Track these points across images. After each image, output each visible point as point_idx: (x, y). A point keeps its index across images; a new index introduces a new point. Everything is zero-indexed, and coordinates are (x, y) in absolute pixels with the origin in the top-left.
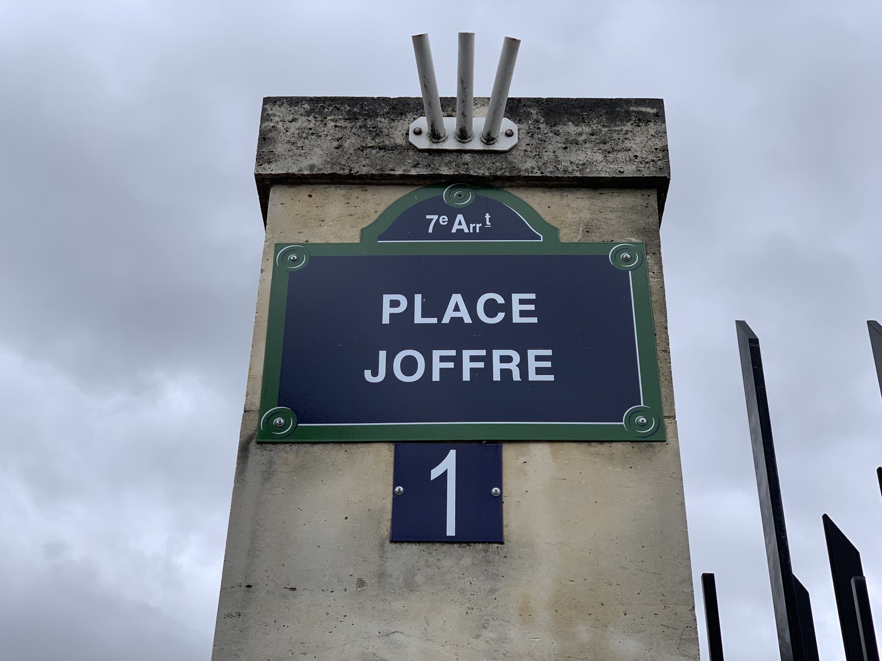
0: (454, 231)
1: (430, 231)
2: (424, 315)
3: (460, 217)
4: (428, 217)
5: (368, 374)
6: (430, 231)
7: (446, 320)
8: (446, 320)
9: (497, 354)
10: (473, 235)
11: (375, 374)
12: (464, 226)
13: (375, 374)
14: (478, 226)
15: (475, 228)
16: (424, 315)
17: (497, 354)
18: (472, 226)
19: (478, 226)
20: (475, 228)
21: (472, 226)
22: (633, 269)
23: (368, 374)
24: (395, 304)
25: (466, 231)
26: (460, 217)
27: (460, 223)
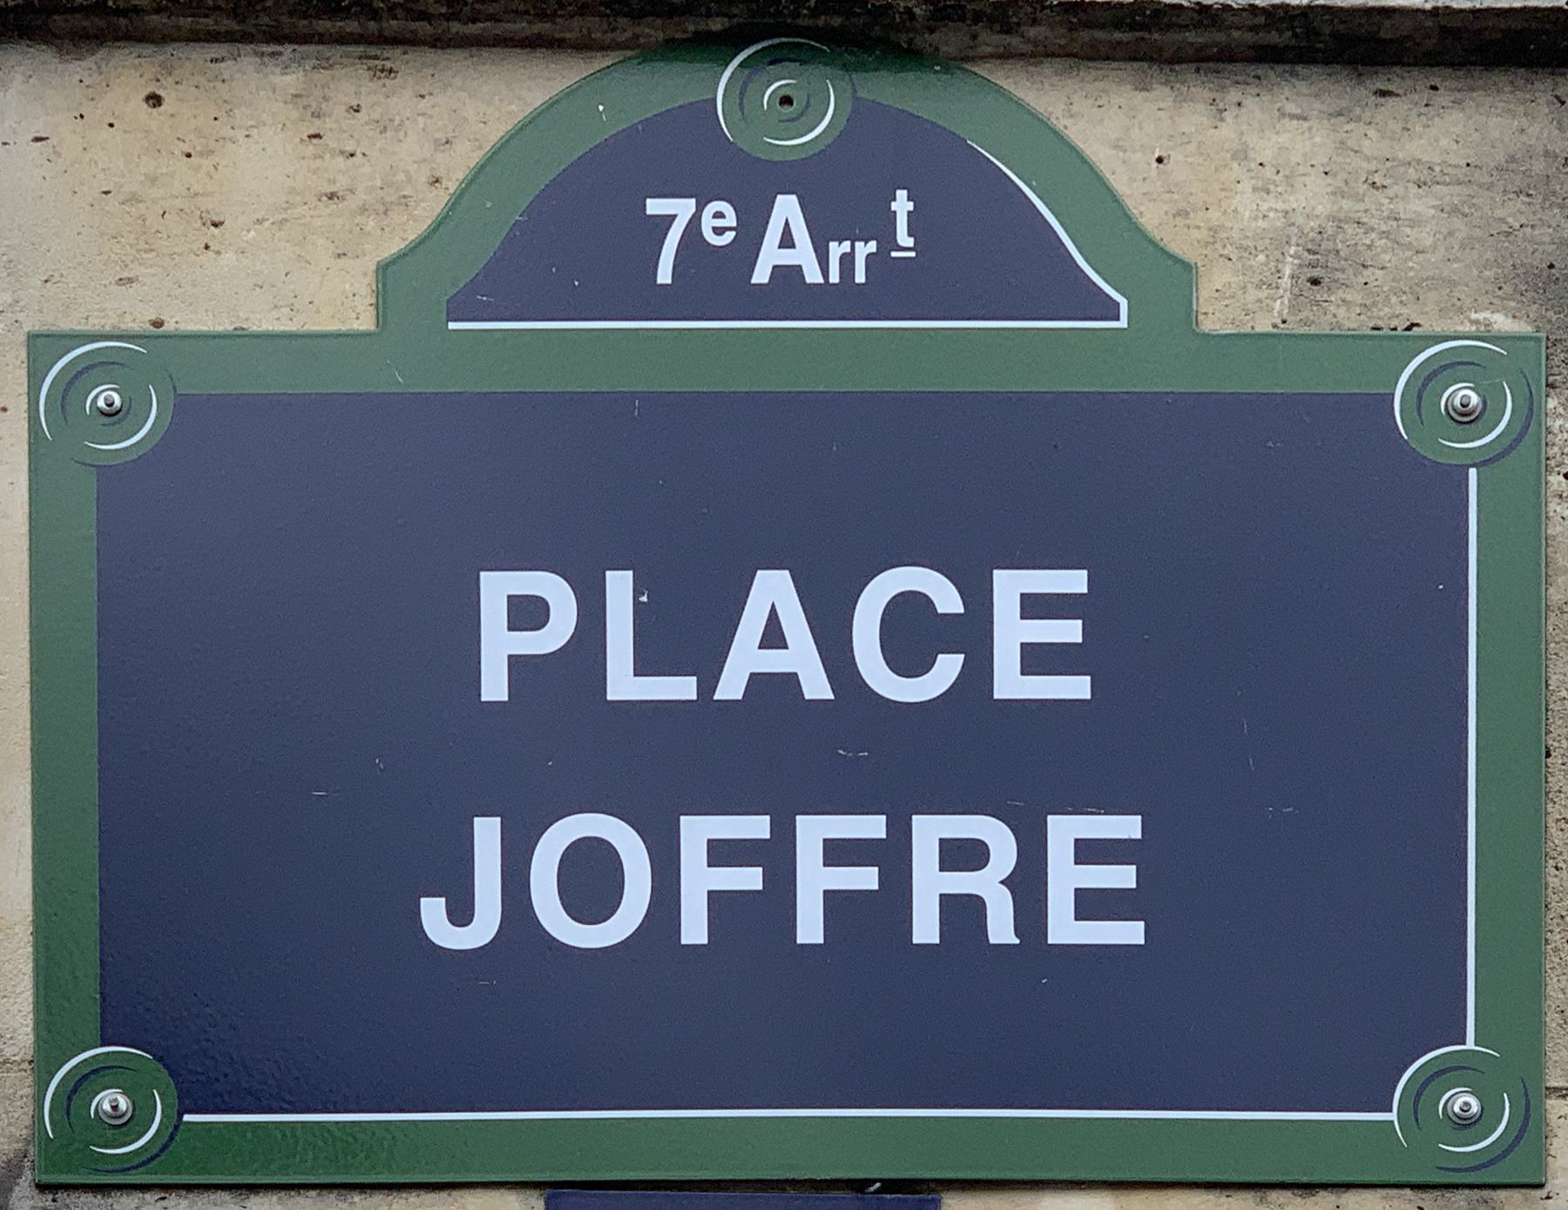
2: (645, 666)
5: (433, 911)
9: (929, 831)
11: (461, 914)
12: (803, 255)
13: (461, 914)
14: (864, 250)
15: (847, 261)
16: (645, 666)
17: (929, 831)
18: (836, 250)
19: (864, 250)
20: (847, 261)
21: (836, 250)
22: (1485, 461)
23: (433, 911)
25: (813, 276)
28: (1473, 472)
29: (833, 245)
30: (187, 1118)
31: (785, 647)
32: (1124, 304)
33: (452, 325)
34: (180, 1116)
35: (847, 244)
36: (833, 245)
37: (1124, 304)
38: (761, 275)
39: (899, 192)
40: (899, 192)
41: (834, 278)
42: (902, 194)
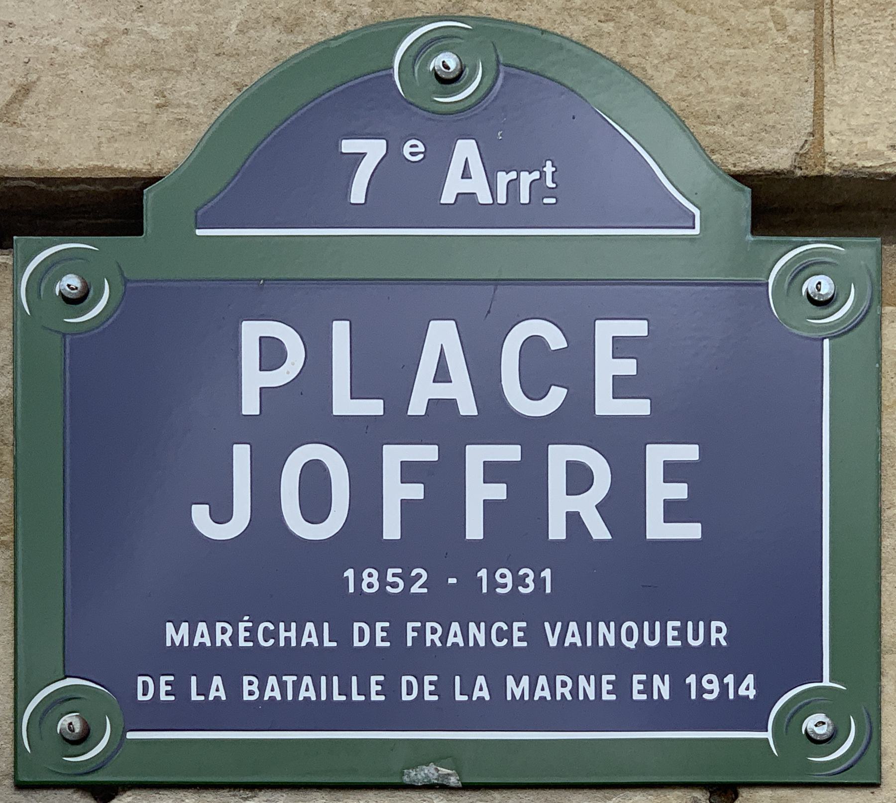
0: (448, 197)
1: (358, 195)
2: (355, 395)
3: (466, 150)
4: (349, 146)
5: (200, 515)
6: (358, 195)
7: (211, 698)
8: (211, 698)
9: (429, 625)
10: (509, 212)
11: (222, 515)
12: (478, 186)
13: (222, 515)
14: (526, 178)
15: (514, 187)
16: (355, 395)
17: (429, 625)
18: (503, 179)
19: (526, 178)
20: (514, 187)
21: (503, 179)
22: (839, 334)
23: (200, 515)
24: (272, 354)
25: (485, 197)
26: (466, 150)
27: (466, 172)
28: (826, 342)
29: (501, 175)
30: (130, 735)
31: (451, 382)
32: (697, 212)
33: (199, 232)
34: (124, 735)
35: (513, 175)
36: (501, 175)
37: (697, 212)
38: (448, 197)
39: (420, 488)
40: (420, 488)
41: (502, 199)
42: (549, 163)
